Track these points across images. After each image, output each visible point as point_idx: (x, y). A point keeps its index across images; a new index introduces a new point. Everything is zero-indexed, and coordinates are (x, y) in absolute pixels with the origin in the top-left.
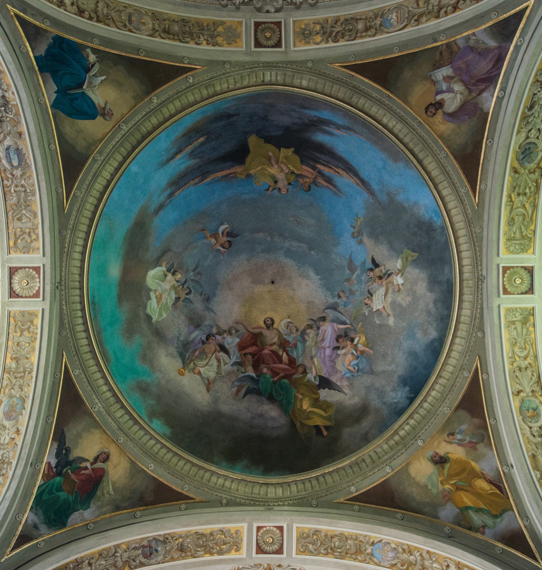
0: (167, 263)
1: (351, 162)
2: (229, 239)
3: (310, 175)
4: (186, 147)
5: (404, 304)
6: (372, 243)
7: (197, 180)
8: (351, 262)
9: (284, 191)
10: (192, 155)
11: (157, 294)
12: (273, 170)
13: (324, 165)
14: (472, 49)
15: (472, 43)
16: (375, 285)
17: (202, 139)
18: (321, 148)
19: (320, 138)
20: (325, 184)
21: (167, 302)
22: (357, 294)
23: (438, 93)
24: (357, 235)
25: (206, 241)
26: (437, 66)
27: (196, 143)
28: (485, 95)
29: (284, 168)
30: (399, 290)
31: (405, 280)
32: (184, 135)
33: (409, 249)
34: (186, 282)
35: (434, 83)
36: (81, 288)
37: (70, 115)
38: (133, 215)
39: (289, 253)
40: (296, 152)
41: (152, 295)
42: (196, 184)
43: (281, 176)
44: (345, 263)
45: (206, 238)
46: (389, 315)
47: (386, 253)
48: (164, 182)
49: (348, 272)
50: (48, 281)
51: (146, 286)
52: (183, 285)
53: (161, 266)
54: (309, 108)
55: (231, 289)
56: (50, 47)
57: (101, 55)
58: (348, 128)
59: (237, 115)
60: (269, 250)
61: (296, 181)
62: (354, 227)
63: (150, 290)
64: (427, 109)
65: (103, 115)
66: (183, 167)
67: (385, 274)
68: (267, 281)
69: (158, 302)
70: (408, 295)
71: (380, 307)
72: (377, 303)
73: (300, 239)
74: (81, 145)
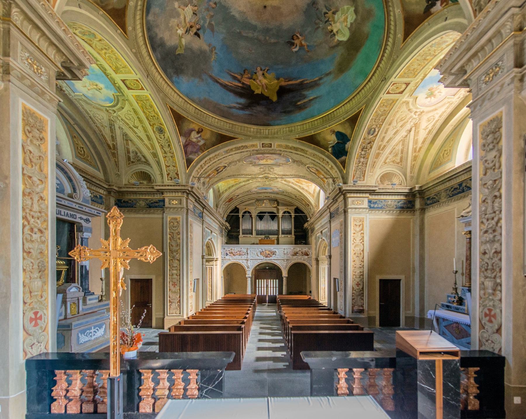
0: (334, 40)
1: (225, 90)
2: (293, 41)
3: (245, 79)
4: (307, 102)
5: (173, 20)
6: (203, 48)
7: (305, 82)
8: (213, 30)
9: (259, 69)
10: (305, 97)
11: (346, 23)
12: (265, 81)
13: (238, 86)
14: (196, 152)
15: (196, 154)
16: (193, 21)
17: (299, 103)
18: (240, 95)
19: (242, 101)
20: (236, 75)
21: (342, 14)
22: (203, 10)
23: (201, 136)
24: (213, 48)
25: (308, 44)
26: (204, 144)
27: (302, 102)
28: (185, 141)
29: (259, 82)
30: (178, 25)
31: (177, 33)
32: (306, 108)
33: (182, 54)
34: (326, 22)
35: (203, 139)
36: (378, 66)
37: (346, 136)
38: (342, 77)
39: (254, 28)
40: (254, 92)
41: (349, 26)
42: (307, 80)
43: (261, 78)
44: (216, 28)
45: (308, 46)
46: (179, 7)
47: (193, 45)
48: (322, 87)
49: (213, 23)
50: (387, 86)
51: (350, 32)
52: (328, 21)
53: (338, 40)
54: (249, 114)
55: (296, 6)
56: (341, 157)
57: (327, 149)
58: (230, 108)
59: (281, 112)
60: (267, 31)
61: (252, 75)
62: (216, 53)
63: (349, 29)
64: (202, 130)
65: (334, 131)
66: (310, 92)
67: (189, 30)
68: (269, 8)
69: (347, 18)
70: (172, 26)
71: (186, 9)
72: (189, 10)
73: (247, 38)
74: (347, 125)
